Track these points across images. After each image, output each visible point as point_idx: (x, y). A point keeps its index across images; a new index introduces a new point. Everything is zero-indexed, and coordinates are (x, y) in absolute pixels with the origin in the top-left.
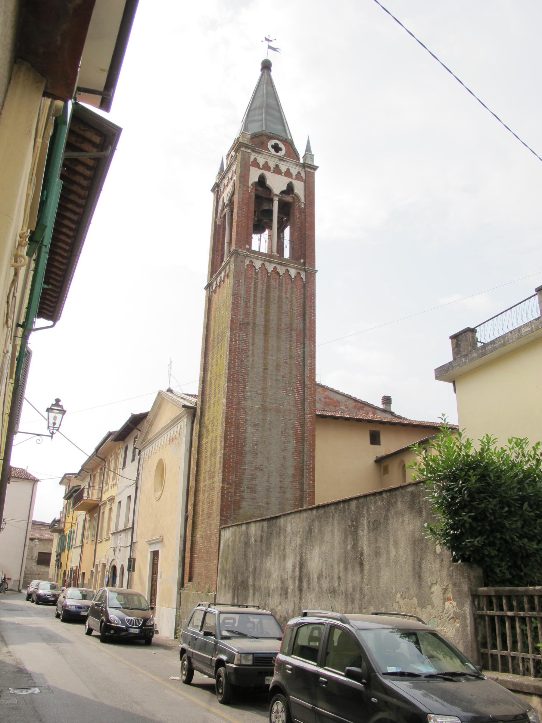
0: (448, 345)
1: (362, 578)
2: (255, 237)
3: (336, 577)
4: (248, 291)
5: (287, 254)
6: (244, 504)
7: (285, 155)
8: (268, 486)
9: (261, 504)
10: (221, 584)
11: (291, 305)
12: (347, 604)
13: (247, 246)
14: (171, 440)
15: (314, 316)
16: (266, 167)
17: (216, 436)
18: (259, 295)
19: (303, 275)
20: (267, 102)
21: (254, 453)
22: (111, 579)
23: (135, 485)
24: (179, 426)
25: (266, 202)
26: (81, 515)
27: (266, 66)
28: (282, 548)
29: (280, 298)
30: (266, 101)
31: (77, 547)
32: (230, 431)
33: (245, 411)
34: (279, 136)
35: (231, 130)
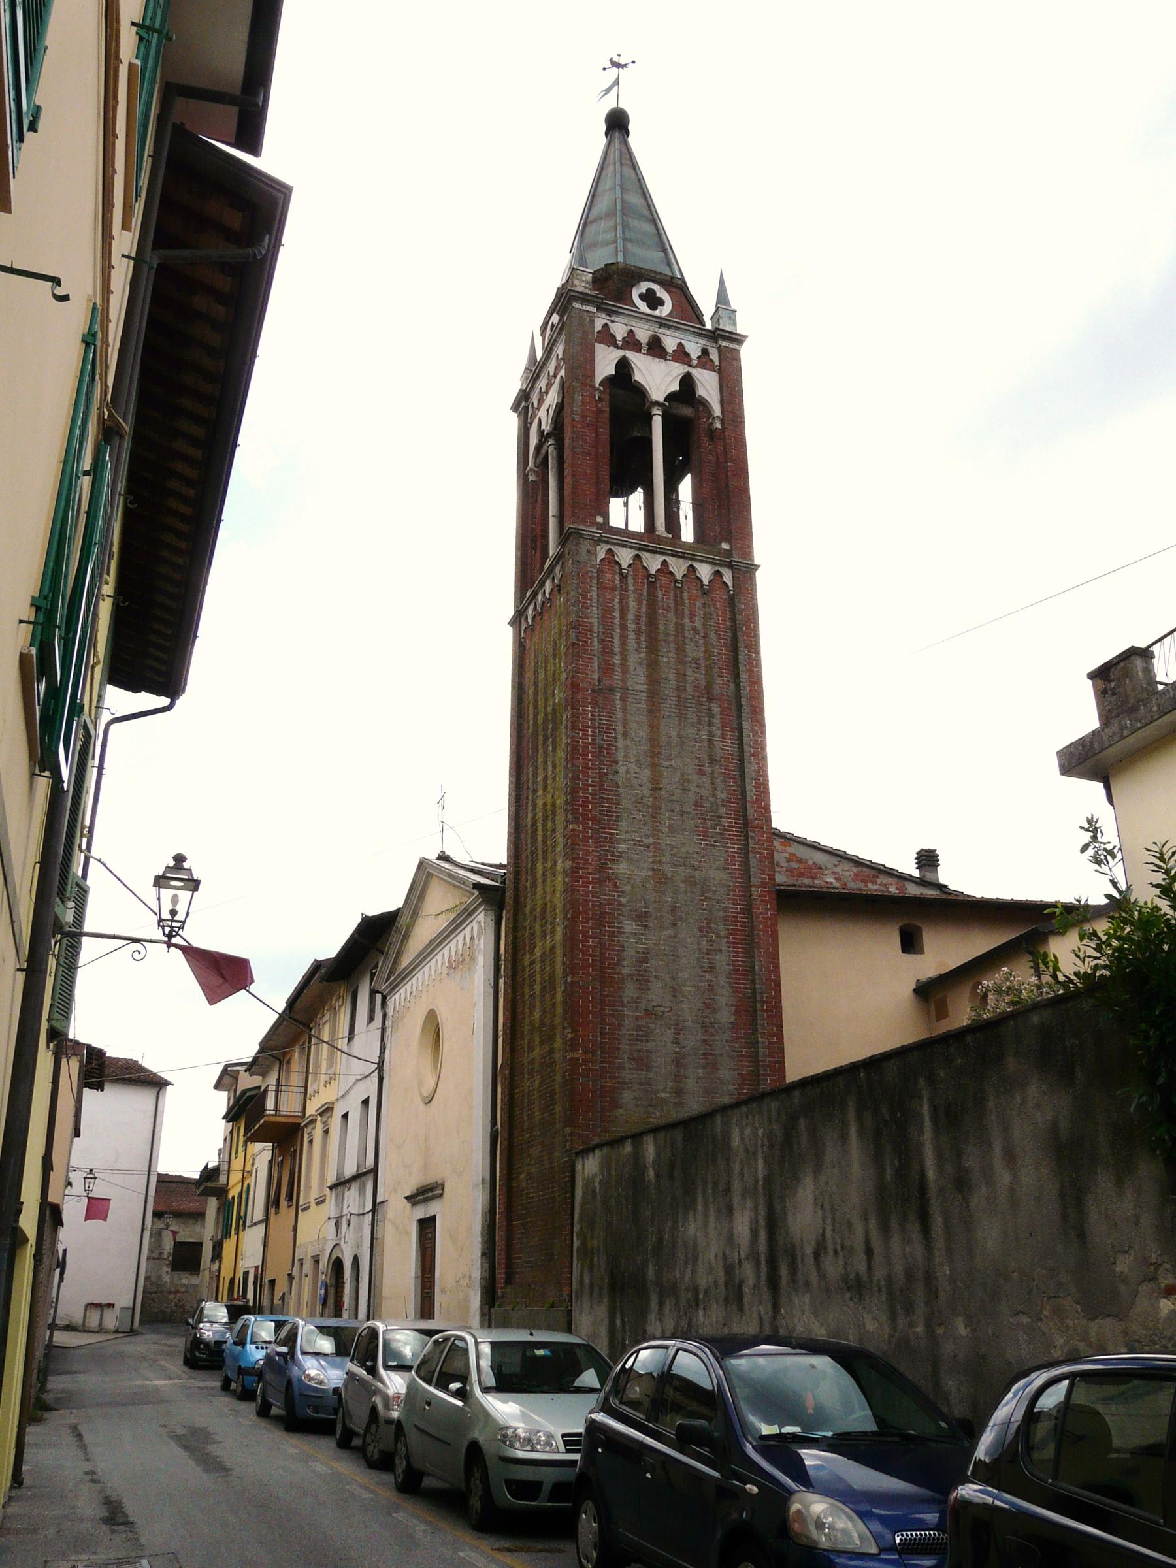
0: (1087, 692)
1: (929, 1248)
2: (616, 505)
3: (860, 1248)
4: (606, 619)
5: (688, 533)
6: (627, 1097)
7: (670, 314)
8: (676, 1052)
9: (663, 1095)
10: (581, 1282)
11: (706, 643)
12: (893, 1317)
13: (600, 520)
14: (453, 966)
15: (759, 666)
16: (631, 342)
17: (553, 948)
18: (631, 626)
19: (728, 577)
20: (623, 201)
21: (642, 980)
22: (332, 1291)
23: (376, 1074)
24: (467, 931)
25: (632, 431)
26: (262, 1153)
27: (617, 123)
28: (721, 1186)
29: (679, 628)
30: (620, 193)
31: (256, 1224)
32: (585, 933)
33: (615, 885)
34: (656, 273)
35: (548, 265)
